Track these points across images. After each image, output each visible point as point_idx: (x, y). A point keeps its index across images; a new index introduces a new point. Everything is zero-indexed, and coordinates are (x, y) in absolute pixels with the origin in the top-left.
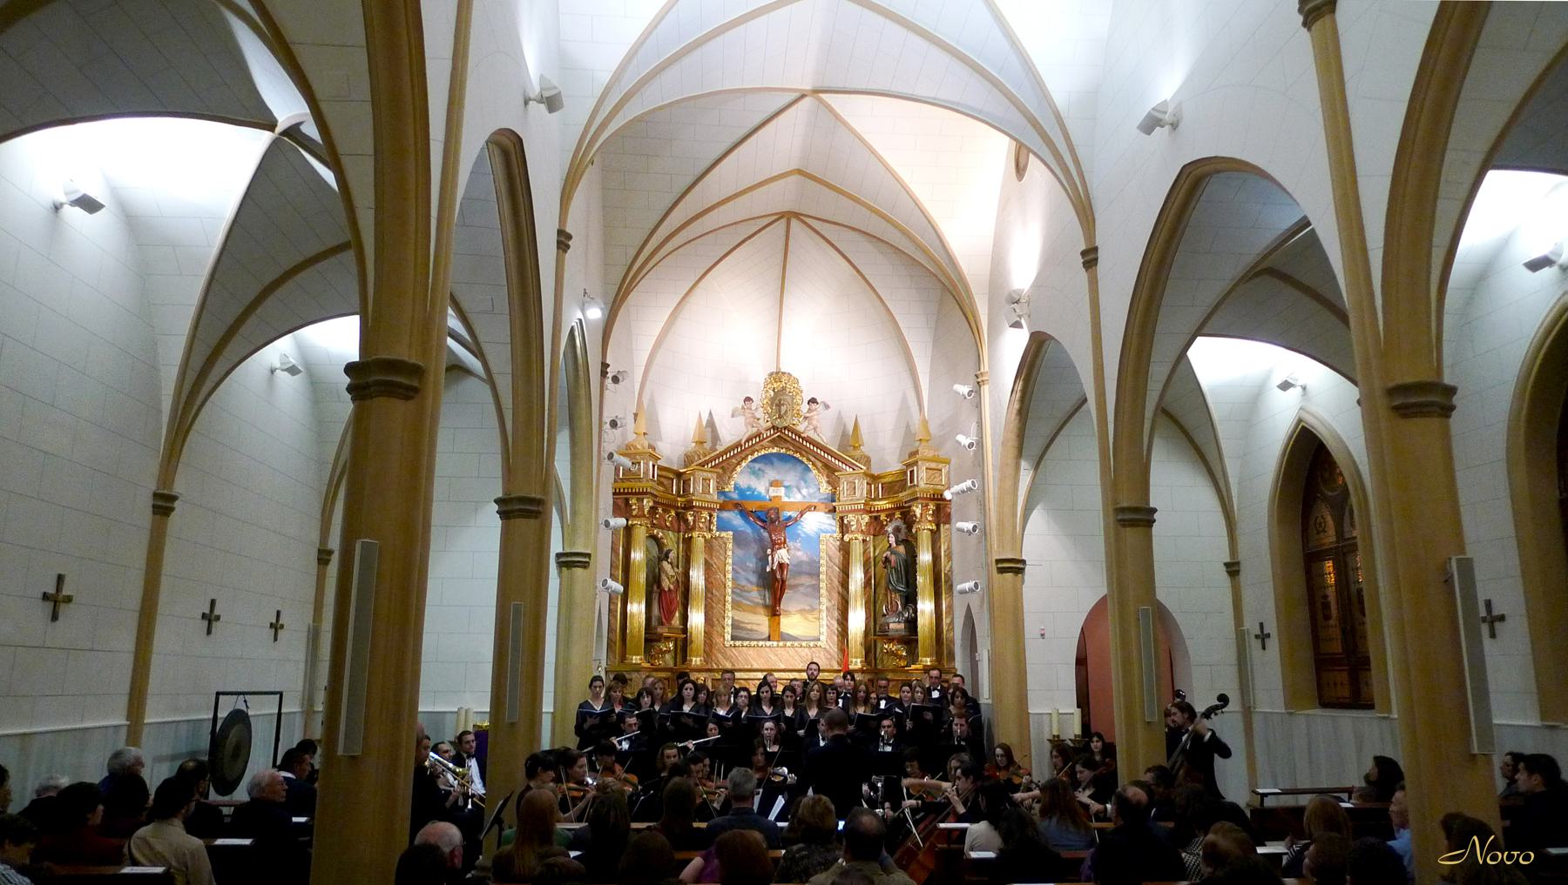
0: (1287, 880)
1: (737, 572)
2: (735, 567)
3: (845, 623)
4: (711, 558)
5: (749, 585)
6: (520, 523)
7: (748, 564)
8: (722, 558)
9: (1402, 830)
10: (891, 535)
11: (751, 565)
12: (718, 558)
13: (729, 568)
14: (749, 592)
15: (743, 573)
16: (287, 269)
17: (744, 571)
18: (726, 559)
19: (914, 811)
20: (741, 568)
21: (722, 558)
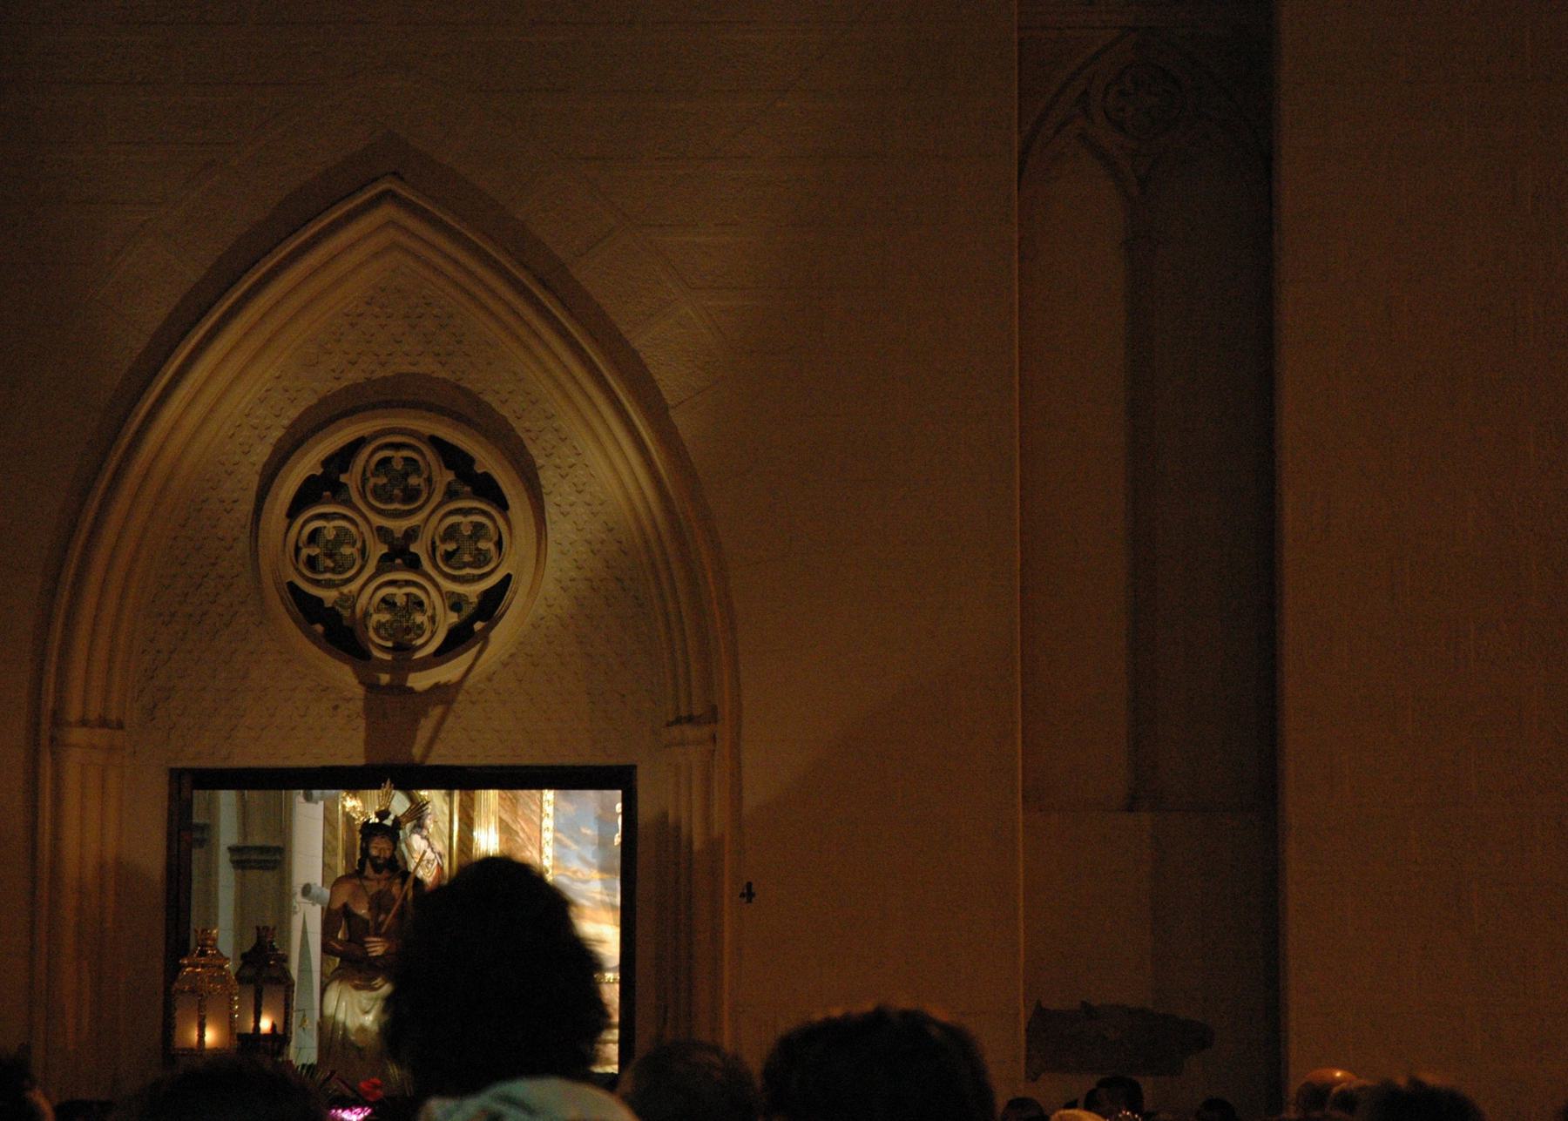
0: (346, 1115)
1: (565, 846)
2: (559, 835)
3: (329, 837)
4: (515, 821)
5: (586, 871)
6: (254, 875)
7: (584, 830)
8: (536, 819)
9: (398, 604)
10: (358, 833)
11: (589, 832)
12: (529, 821)
13: (548, 836)
14: (586, 882)
15: (574, 847)
16: (541, 473)
17: (577, 842)
18: (541, 819)
19: (387, 912)
20: (571, 837)
21: (536, 819)
